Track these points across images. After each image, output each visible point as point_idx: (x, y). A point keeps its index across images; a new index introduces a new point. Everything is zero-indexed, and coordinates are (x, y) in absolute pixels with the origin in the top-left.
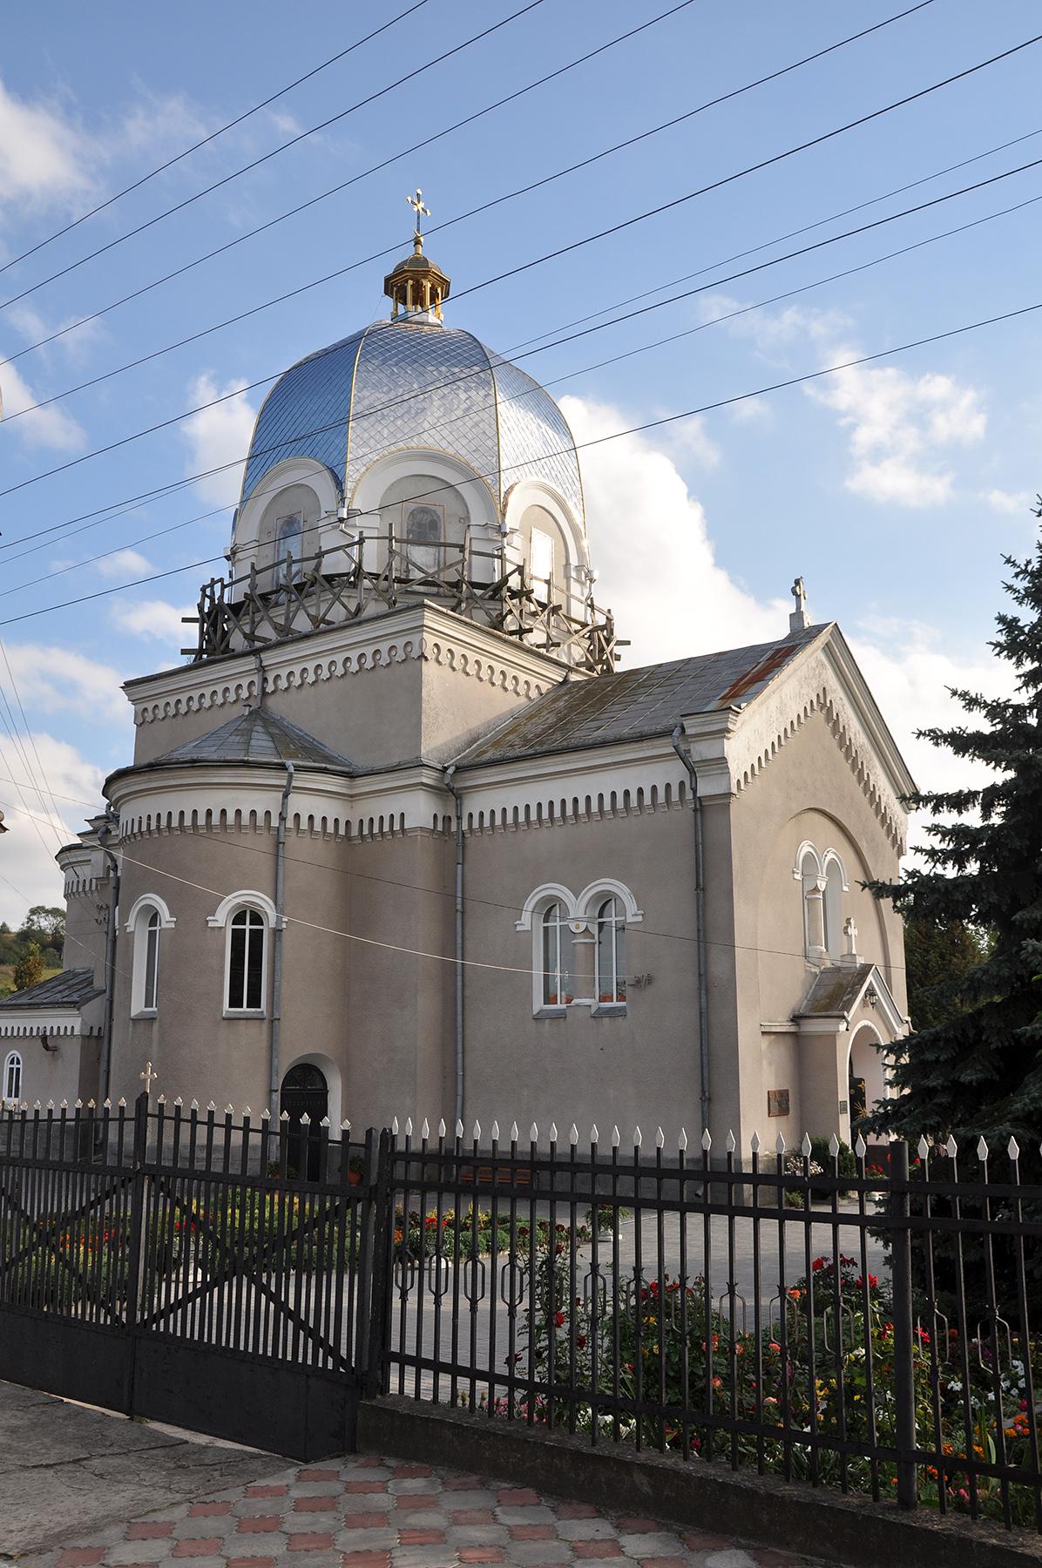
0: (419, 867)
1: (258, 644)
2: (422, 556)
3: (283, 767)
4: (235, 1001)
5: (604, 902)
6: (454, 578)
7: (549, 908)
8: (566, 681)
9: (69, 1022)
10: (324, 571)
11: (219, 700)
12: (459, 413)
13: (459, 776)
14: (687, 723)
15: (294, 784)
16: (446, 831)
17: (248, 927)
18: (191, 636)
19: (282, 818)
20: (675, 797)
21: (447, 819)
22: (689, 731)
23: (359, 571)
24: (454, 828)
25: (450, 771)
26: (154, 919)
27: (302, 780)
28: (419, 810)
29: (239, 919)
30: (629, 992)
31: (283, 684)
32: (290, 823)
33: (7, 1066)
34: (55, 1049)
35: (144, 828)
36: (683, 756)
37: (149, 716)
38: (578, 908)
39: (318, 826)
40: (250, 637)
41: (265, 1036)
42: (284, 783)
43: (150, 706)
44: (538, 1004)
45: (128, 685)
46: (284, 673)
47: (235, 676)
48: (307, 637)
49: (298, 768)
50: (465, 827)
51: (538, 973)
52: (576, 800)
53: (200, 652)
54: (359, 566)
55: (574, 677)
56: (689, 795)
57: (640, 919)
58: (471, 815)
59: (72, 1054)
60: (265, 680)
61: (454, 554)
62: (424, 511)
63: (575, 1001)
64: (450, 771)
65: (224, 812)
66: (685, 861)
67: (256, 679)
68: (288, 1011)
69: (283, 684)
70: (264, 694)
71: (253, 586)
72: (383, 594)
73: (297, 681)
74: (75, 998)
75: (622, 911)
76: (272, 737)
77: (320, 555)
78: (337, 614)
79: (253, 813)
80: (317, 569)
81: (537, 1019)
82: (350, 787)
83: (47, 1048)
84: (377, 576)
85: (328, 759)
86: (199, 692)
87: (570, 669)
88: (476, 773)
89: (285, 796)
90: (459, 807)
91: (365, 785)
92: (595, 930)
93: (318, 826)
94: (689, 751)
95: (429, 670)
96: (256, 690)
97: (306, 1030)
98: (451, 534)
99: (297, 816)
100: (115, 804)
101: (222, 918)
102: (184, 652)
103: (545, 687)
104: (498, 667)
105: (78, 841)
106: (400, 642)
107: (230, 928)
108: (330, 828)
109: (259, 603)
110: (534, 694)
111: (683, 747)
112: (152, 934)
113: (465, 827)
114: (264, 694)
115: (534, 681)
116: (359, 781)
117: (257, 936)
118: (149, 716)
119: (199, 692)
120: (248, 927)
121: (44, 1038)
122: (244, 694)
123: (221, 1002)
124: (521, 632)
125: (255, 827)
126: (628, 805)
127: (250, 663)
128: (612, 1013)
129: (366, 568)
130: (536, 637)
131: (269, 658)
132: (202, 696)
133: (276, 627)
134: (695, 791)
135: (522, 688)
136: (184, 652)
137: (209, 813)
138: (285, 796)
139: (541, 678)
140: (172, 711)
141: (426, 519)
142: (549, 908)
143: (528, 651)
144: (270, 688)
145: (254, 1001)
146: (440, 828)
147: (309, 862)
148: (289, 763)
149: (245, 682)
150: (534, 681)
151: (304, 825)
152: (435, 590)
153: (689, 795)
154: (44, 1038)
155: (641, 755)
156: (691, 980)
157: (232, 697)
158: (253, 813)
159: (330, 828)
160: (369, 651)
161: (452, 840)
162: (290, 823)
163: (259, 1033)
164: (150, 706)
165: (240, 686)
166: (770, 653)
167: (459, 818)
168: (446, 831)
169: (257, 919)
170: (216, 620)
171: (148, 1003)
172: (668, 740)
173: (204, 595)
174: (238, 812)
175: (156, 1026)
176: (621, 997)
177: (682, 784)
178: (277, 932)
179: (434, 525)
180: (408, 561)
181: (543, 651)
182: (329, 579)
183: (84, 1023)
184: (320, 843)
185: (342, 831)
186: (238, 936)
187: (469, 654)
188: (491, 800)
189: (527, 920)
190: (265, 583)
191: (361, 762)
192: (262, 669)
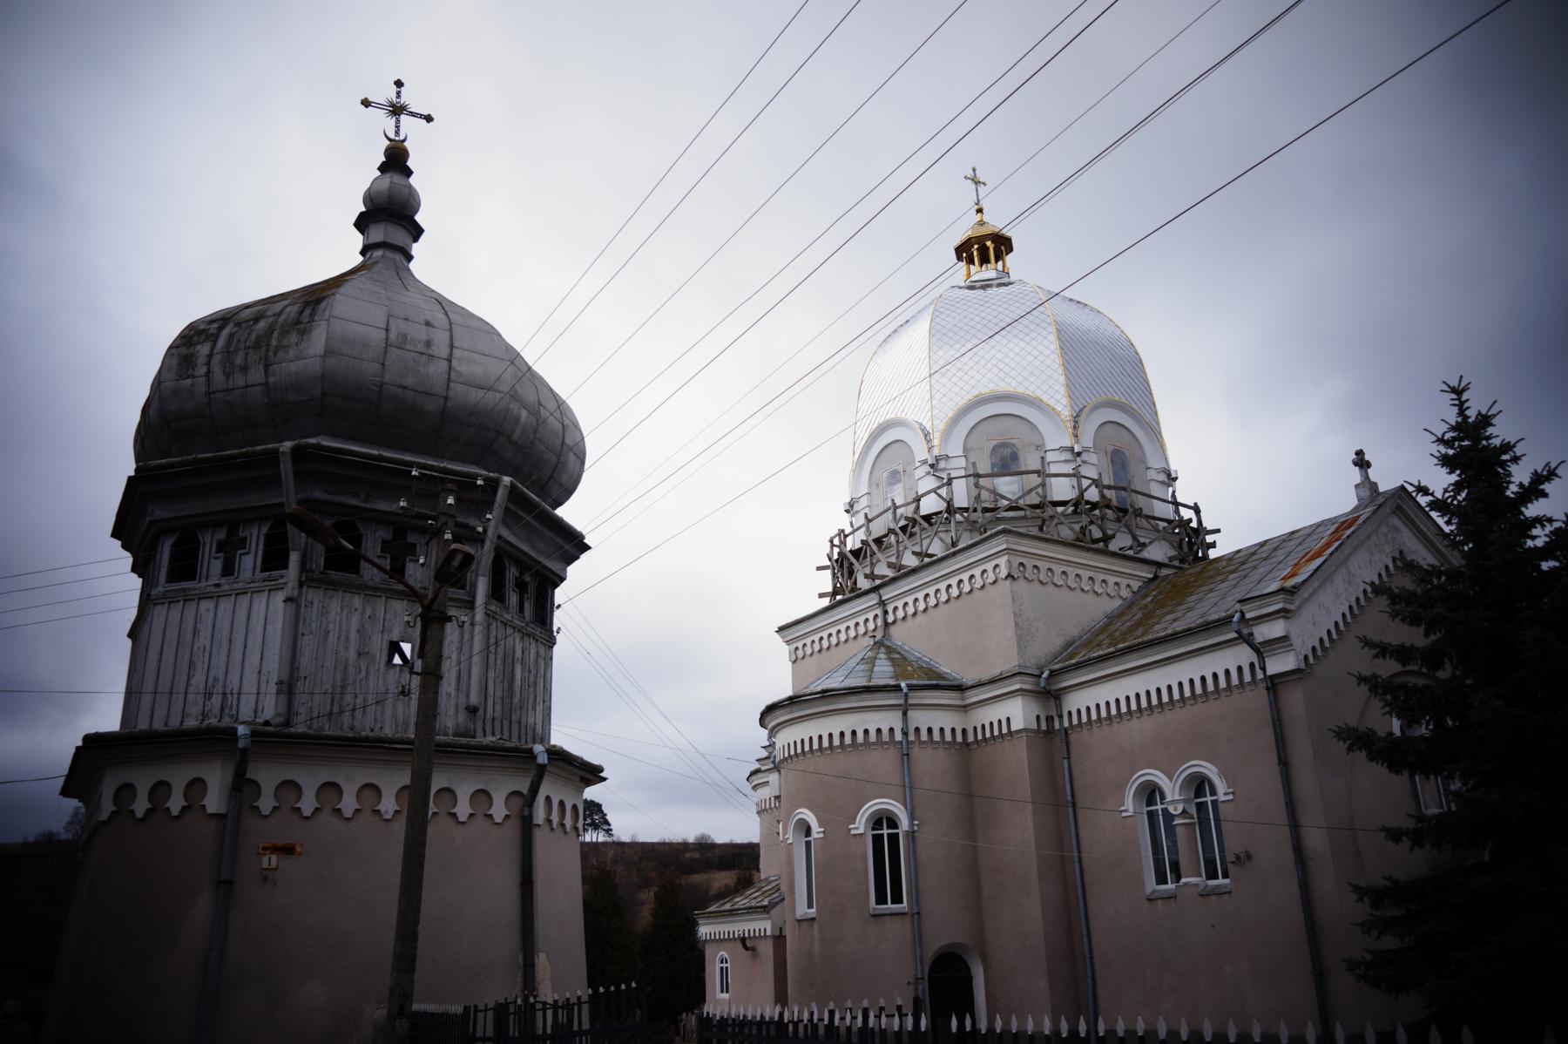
0: (1017, 764)
1: (878, 582)
2: (1008, 486)
3: (897, 688)
4: (881, 899)
5: (1199, 785)
6: (1036, 501)
8: (1156, 577)
9: (764, 926)
10: (923, 512)
16: (1050, 731)
17: (885, 832)
18: (826, 582)
19: (905, 733)
20: (1247, 678)
21: (1049, 719)
22: (1248, 616)
23: (951, 509)
24: (1057, 726)
25: (1045, 675)
26: (808, 831)
27: (916, 698)
28: (1017, 713)
30: (1231, 868)
31: (900, 614)
32: (912, 737)
33: (718, 966)
36: (1248, 640)
37: (800, 653)
38: (1172, 790)
39: (936, 737)
40: (871, 576)
42: (901, 701)
43: (800, 645)
44: (1150, 884)
45: (781, 629)
46: (900, 604)
47: (863, 613)
48: (914, 571)
50: (1066, 724)
51: (1076, 854)
52: (1159, 690)
53: (835, 593)
54: (949, 503)
56: (1260, 675)
57: (1230, 797)
58: (1070, 713)
59: (766, 949)
60: (886, 612)
61: (1035, 480)
62: (1003, 445)
63: (1184, 880)
64: (1045, 675)
66: (1267, 738)
67: (879, 612)
69: (900, 614)
70: (886, 624)
71: (869, 532)
72: (973, 526)
73: (911, 610)
74: (765, 903)
75: (1213, 792)
76: (892, 660)
77: (918, 500)
78: (937, 548)
79: (879, 731)
80: (918, 508)
83: (746, 948)
84: (966, 510)
85: (940, 676)
86: (957, 579)
89: (905, 714)
90: (1059, 707)
91: (974, 697)
92: (1194, 811)
93: (936, 737)
94: (1251, 634)
96: (880, 622)
98: (1030, 461)
99: (917, 729)
100: (773, 733)
101: (860, 825)
102: (821, 596)
103: (1136, 585)
105: (757, 766)
107: (870, 833)
108: (948, 737)
109: (874, 547)
110: (1125, 593)
111: (1245, 631)
112: (808, 844)
113: (1066, 724)
115: (1132, 583)
116: (968, 693)
117: (894, 839)
118: (800, 653)
119: (957, 579)
122: (871, 626)
123: (867, 900)
124: (1107, 539)
126: (1205, 693)
127: (873, 599)
128: (1218, 893)
129: (957, 504)
130: (1121, 541)
131: (887, 594)
133: (890, 565)
134: (1264, 669)
135: (1111, 590)
136: (821, 596)
137: (842, 734)
138: (905, 714)
141: (1007, 451)
143: (1114, 555)
144: (890, 619)
145: (897, 899)
146: (1044, 727)
147: (933, 767)
148: (903, 685)
149: (870, 616)
150: (1124, 582)
151: (924, 736)
152: (1022, 513)
153: (1260, 675)
154: (743, 940)
156: (1288, 855)
157: (862, 630)
158: (879, 731)
159: (948, 737)
160: (965, 576)
161: (1053, 739)
162: (912, 737)
164: (800, 645)
165: (949, 586)
166: (1333, 528)
167: (1061, 717)
168: (1050, 731)
169: (893, 823)
170: (844, 564)
171: (810, 906)
173: (833, 545)
174: (866, 732)
175: (816, 926)
176: (1226, 876)
177: (1252, 665)
178: (911, 835)
179: (1014, 457)
180: (994, 492)
181: (1130, 553)
182: (927, 518)
183: (773, 925)
184: (941, 752)
185: (959, 738)
186: (877, 840)
187: (1054, 567)
188: (1089, 698)
190: (878, 529)
191: (969, 678)
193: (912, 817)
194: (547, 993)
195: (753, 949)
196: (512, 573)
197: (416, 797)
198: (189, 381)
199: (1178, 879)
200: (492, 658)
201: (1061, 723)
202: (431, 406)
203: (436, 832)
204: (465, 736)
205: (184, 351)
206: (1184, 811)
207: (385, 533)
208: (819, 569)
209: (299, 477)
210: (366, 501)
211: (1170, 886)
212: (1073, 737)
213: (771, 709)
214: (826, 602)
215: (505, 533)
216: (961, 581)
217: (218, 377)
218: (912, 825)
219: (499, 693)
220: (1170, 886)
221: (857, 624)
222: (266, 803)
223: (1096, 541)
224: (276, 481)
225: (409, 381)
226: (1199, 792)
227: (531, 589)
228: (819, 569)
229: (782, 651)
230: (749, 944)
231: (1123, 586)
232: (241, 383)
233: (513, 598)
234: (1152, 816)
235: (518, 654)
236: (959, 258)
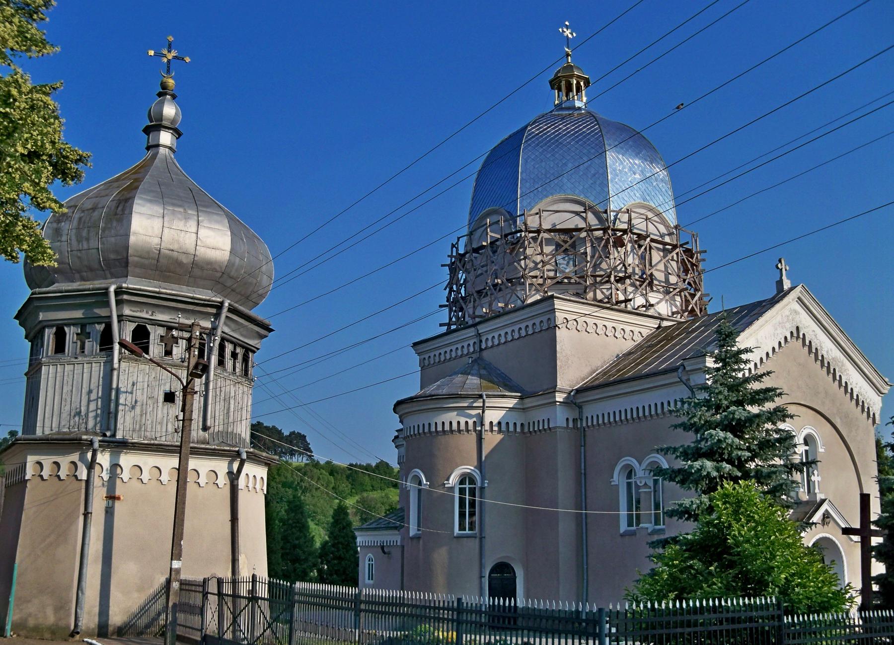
1: (477, 320)
4: (462, 527)
7: (630, 472)
8: (659, 327)
11: (459, 353)
12: (581, 167)
13: (578, 395)
14: (686, 363)
15: (487, 405)
17: (467, 486)
18: (444, 316)
21: (575, 420)
22: (688, 368)
29: (462, 482)
33: (367, 562)
34: (389, 553)
35: (421, 431)
37: (426, 362)
41: (196, 627)
45: (415, 344)
46: (490, 337)
49: (488, 396)
50: (584, 425)
55: (665, 324)
59: (396, 554)
60: (481, 341)
65: (451, 423)
68: (488, 531)
81: (622, 535)
82: (523, 404)
83: (384, 552)
87: (663, 319)
88: (589, 393)
90: (581, 413)
94: (689, 379)
95: (561, 334)
97: (502, 544)
101: (453, 480)
102: (441, 325)
104: (610, 325)
106: (545, 318)
108: (511, 428)
111: (684, 378)
112: (420, 491)
113: (584, 425)
114: (481, 350)
115: (642, 330)
120: (467, 486)
121: (382, 548)
125: (468, 431)
131: (482, 328)
132: (520, 329)
136: (441, 325)
139: (646, 327)
140: (523, 333)
142: (630, 472)
144: (483, 346)
150: (636, 330)
155: (651, 385)
159: (511, 428)
162: (487, 427)
163: (474, 544)
164: (426, 356)
167: (581, 420)
169: (472, 481)
172: (675, 374)
178: (482, 488)
185: (518, 430)
189: (618, 478)
192: (479, 335)
193: (483, 478)
194: (245, 573)
195: (389, 553)
196: (229, 348)
197: (181, 472)
198: (59, 244)
199: (638, 524)
200: (218, 400)
201: (581, 424)
202: (184, 259)
203: (191, 487)
204: (203, 443)
205: (55, 225)
206: (646, 484)
207: (161, 331)
208: (441, 306)
209: (119, 303)
210: (152, 315)
211: (634, 528)
212: (588, 433)
213: (399, 403)
214: (444, 329)
215: (226, 330)
216: (527, 326)
217: (74, 243)
218: (483, 483)
219: (221, 417)
220: (634, 528)
221: (463, 347)
222: (125, 476)
223: (618, 302)
224: (107, 304)
225: (175, 247)
226: (629, 476)
227: (240, 357)
228: (441, 306)
229: (414, 360)
230: (386, 550)
231: (636, 333)
232: (85, 246)
233: (229, 363)
234: (629, 485)
235: (232, 394)
236: (553, 88)
